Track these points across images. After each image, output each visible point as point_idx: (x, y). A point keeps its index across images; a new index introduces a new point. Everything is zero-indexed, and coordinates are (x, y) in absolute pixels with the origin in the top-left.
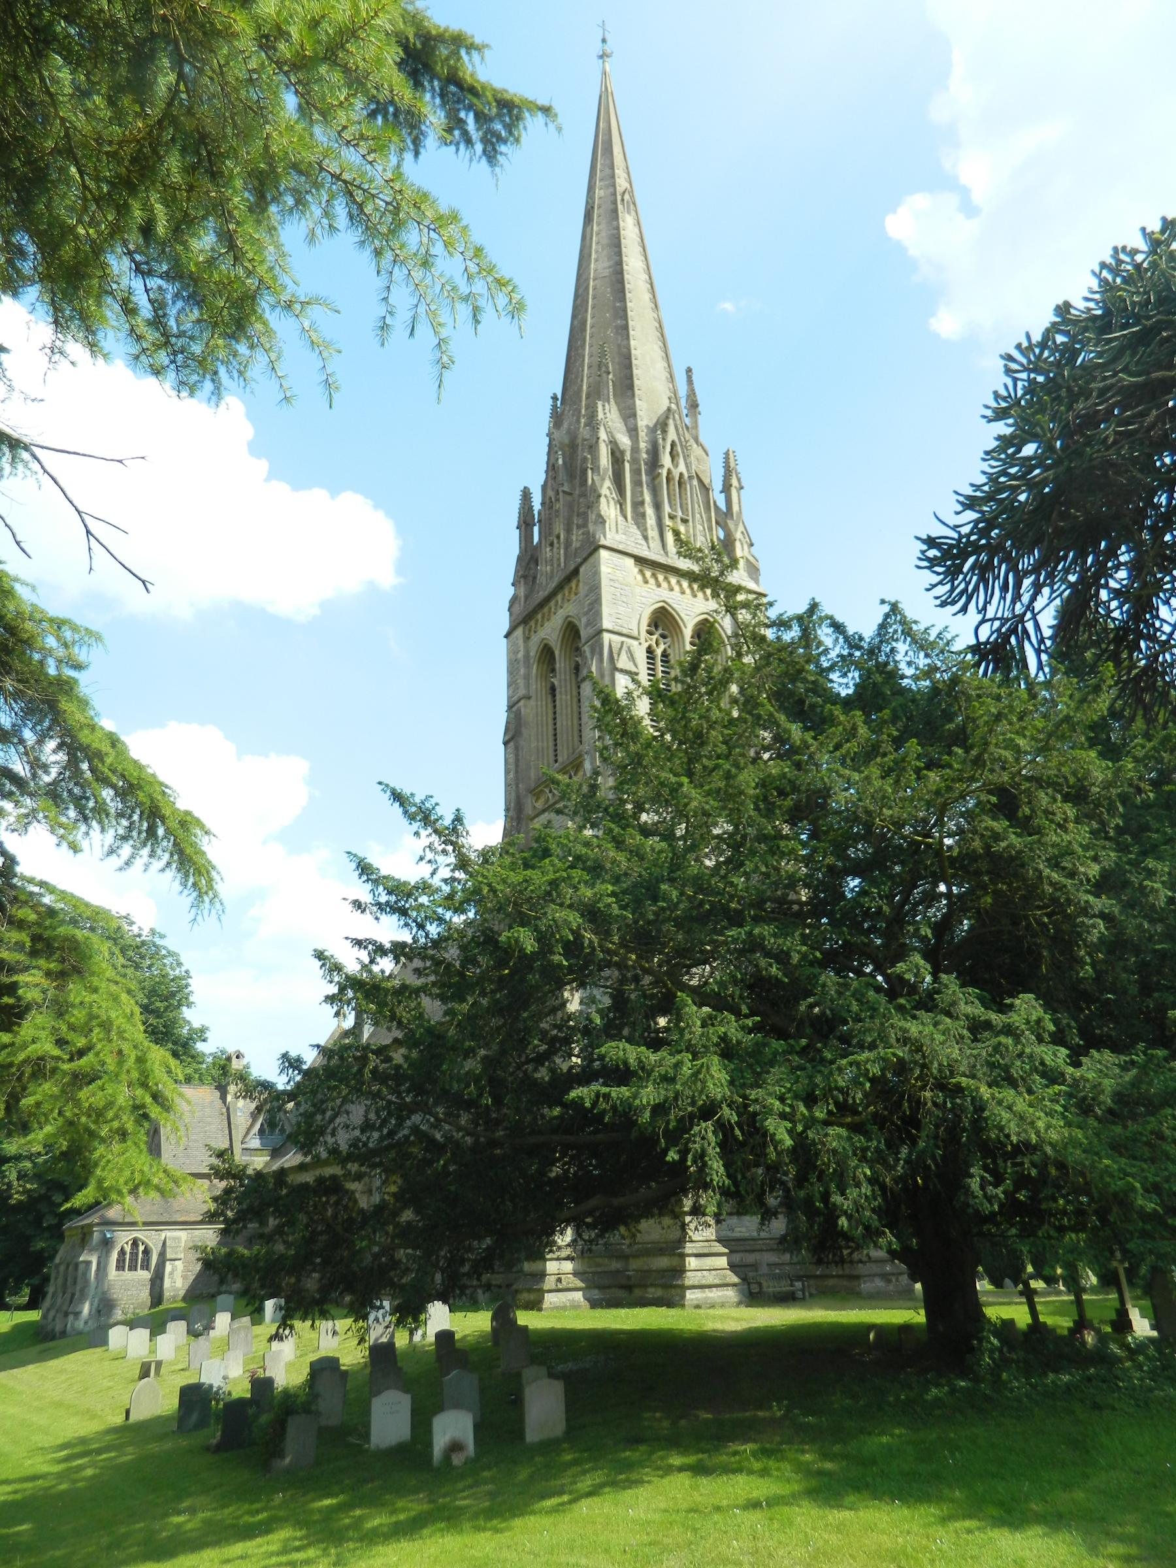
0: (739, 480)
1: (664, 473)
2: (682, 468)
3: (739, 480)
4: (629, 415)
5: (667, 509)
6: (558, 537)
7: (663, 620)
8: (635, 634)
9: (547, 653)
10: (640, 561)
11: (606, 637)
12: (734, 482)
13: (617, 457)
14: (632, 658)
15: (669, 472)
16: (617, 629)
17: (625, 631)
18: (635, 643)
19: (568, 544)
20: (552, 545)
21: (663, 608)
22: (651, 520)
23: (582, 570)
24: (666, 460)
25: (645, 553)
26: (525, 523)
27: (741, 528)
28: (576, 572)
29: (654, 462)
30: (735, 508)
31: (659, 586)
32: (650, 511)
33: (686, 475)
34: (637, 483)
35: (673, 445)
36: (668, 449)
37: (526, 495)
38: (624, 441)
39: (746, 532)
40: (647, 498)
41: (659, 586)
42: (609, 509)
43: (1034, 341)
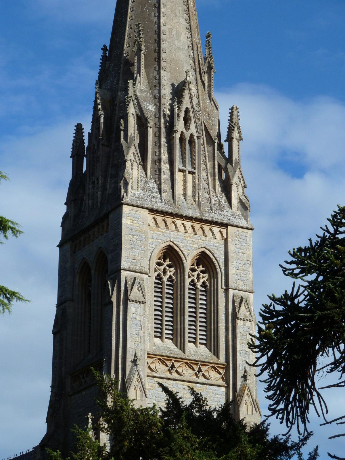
0: (239, 132)
1: (178, 136)
2: (193, 129)
3: (239, 132)
4: (156, 84)
5: (178, 165)
6: (98, 179)
7: (171, 254)
8: (147, 269)
9: (85, 267)
10: (152, 211)
11: (123, 273)
12: (235, 135)
13: (142, 122)
14: (142, 290)
15: (182, 134)
16: (132, 267)
17: (138, 269)
18: (145, 276)
19: (104, 189)
20: (93, 183)
21: (169, 246)
22: (165, 176)
23: (111, 216)
24: (180, 125)
25: (159, 206)
26: (77, 153)
27: (238, 173)
28: (107, 216)
29: (171, 129)
30: (235, 156)
31: (167, 228)
32: (165, 167)
33: (195, 135)
34: (158, 145)
35: (187, 111)
36: (183, 115)
37: (79, 128)
38: (150, 107)
39: (242, 178)
40: (165, 156)
41: (167, 228)
42: (133, 171)
43: (296, 267)
